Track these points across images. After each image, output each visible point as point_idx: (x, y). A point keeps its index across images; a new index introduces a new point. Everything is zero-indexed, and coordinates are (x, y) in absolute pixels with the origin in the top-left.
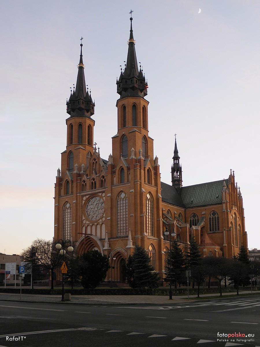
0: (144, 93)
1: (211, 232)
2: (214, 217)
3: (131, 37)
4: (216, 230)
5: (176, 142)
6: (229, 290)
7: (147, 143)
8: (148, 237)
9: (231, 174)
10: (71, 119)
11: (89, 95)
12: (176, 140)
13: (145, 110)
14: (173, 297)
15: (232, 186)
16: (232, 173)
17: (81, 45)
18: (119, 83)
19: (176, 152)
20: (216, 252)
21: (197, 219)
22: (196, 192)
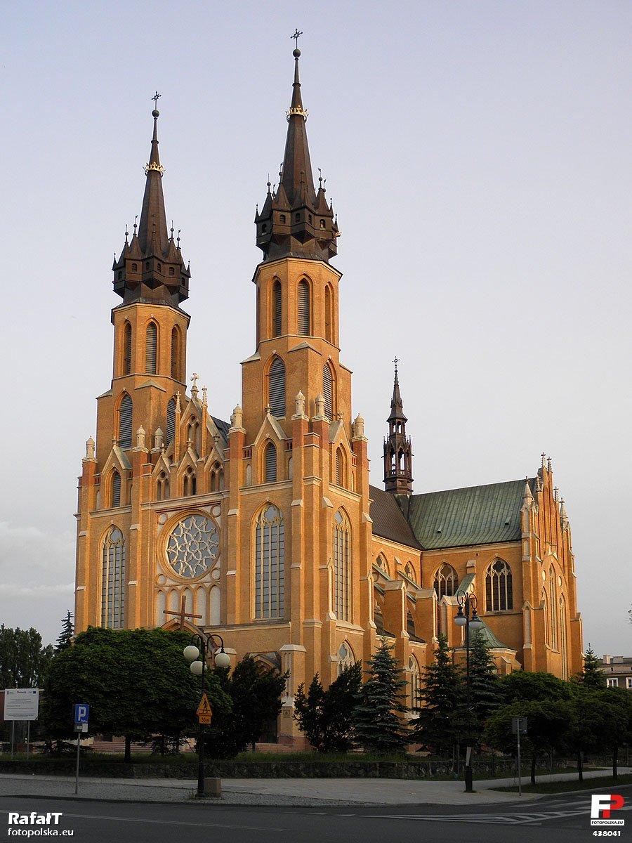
0: (330, 250)
1: (490, 613)
2: (499, 575)
3: (154, 157)
4: (503, 608)
5: (396, 378)
6: (565, 764)
7: (336, 381)
8: (337, 625)
10: (126, 310)
12: (396, 374)
13: (330, 291)
15: (547, 497)
17: (155, 114)
18: (263, 221)
19: (396, 404)
20: (507, 665)
22: (450, 511)
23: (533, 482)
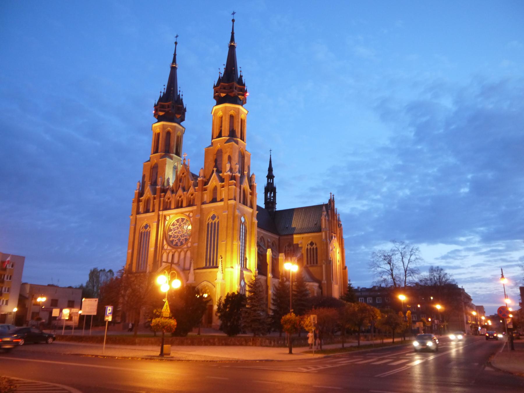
2: (312, 248)
3: (232, 40)
4: (314, 263)
9: (331, 199)
11: (181, 98)
14: (294, 350)
16: (332, 197)
17: (176, 43)
19: (270, 170)
21: (315, 248)
23: (326, 205)
